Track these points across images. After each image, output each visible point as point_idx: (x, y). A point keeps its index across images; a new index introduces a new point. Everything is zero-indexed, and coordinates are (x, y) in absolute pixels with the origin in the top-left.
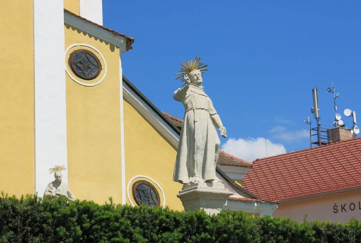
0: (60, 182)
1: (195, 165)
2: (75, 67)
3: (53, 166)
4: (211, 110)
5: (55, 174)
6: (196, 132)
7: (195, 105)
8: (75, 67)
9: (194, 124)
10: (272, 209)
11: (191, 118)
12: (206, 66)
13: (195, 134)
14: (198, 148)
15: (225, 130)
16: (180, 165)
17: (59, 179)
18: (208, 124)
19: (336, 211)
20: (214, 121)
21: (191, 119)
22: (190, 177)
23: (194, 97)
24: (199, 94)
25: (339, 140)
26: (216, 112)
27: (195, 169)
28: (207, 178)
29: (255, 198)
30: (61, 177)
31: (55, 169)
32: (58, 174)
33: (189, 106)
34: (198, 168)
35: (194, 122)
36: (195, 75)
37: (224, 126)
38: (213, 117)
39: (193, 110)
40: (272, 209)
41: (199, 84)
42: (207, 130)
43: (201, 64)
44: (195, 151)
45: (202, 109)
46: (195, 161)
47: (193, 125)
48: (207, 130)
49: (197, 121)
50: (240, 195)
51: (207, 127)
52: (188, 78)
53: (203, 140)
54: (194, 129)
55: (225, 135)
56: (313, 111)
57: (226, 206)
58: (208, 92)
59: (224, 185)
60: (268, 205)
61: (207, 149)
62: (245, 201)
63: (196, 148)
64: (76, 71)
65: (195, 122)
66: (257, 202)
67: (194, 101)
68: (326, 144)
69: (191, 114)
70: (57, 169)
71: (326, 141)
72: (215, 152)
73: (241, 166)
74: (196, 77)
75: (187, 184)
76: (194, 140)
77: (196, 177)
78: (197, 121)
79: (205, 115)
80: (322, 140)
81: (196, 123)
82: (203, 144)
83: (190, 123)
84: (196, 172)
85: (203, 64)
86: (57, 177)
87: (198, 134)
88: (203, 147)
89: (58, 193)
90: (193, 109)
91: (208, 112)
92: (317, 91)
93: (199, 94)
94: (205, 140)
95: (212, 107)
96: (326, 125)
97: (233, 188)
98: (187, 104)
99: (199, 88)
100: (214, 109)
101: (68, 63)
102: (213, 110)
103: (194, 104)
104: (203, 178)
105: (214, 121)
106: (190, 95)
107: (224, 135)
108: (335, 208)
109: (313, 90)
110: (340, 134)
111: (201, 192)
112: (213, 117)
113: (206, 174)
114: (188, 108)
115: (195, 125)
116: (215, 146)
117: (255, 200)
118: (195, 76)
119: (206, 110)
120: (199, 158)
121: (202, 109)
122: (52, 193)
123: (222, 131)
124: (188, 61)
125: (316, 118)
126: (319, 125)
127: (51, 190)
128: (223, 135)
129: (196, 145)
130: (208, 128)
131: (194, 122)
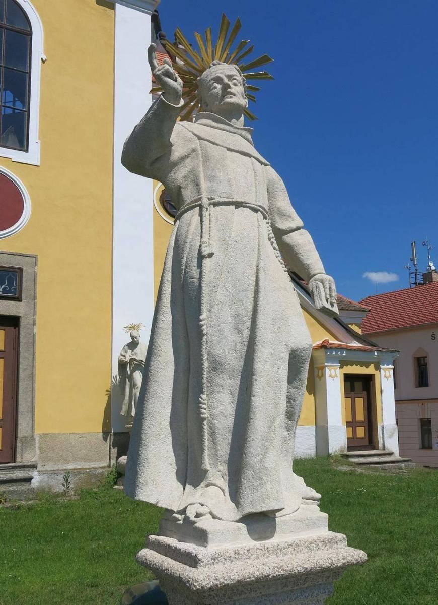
0: (138, 344)
1: (206, 437)
2: (168, 207)
3: (128, 325)
4: (283, 215)
5: (131, 334)
6: (205, 300)
7: (211, 191)
8: (168, 207)
9: (200, 265)
10: (393, 357)
11: (188, 241)
12: (265, 59)
13: (205, 307)
14: (216, 366)
15: (334, 287)
16: (143, 436)
17: (136, 340)
18: (262, 265)
19: (434, 338)
20: (289, 254)
21: (188, 246)
22: (188, 486)
23: (206, 159)
24: (229, 149)
25: (432, 281)
26: (299, 222)
27: (207, 453)
28: (254, 503)
29: (374, 346)
30: (138, 338)
31: (130, 327)
32: (135, 333)
33: (188, 194)
34: (217, 450)
35: (201, 257)
36: (218, 80)
37: (328, 271)
38: (287, 238)
39: (198, 209)
40: (393, 357)
41: (228, 113)
42: (257, 292)
43: (245, 49)
44: (205, 381)
45: (238, 205)
46: (204, 419)
47: (195, 272)
48: (257, 292)
49: (211, 255)
50: (359, 342)
51: (254, 279)
52: (172, 70)
53: (239, 331)
54: (200, 287)
55: (332, 305)
56: (412, 260)
57: (345, 356)
58: (270, 147)
59: (326, 515)
60: (389, 354)
61: (253, 374)
62: (365, 351)
63: (206, 364)
64: (170, 211)
65: (204, 257)
66: (377, 351)
67: (206, 176)
68: (422, 284)
69: (189, 224)
70: (133, 327)
71: (422, 282)
72: (290, 381)
73: (360, 311)
74: (219, 86)
75: (172, 512)
76: (200, 334)
77: (207, 486)
78: (211, 255)
79: (250, 228)
80: (418, 282)
81: (207, 263)
82: (238, 348)
83: (184, 260)
84: (207, 463)
85: (250, 50)
86: (133, 337)
87: (216, 308)
88: (233, 360)
89: (134, 357)
90: (201, 206)
91: (265, 218)
92: (415, 244)
93: (229, 149)
94: (246, 333)
95: (284, 202)
96: (422, 270)
97: (352, 337)
98: (180, 187)
99: (232, 129)
100: (291, 211)
101: (160, 200)
102: (290, 216)
103: (204, 185)
104: (235, 495)
105: (289, 254)
106: (194, 150)
107: (328, 306)
108: (434, 338)
109: (412, 244)
110: (433, 277)
111: (211, 589)
112: (287, 238)
113: (245, 483)
114: (183, 201)
115: (201, 272)
116: (288, 358)
117: (374, 348)
118: (216, 85)
119: (256, 211)
120: (219, 406)
121: (238, 205)
122: (125, 358)
123: (319, 293)
124: (196, 34)
125: (414, 265)
126: (416, 270)
127: (125, 354)
128: (324, 307)
129: (210, 354)
130: (261, 283)
131: (201, 257)
